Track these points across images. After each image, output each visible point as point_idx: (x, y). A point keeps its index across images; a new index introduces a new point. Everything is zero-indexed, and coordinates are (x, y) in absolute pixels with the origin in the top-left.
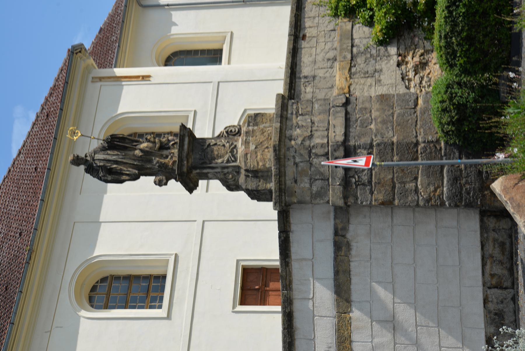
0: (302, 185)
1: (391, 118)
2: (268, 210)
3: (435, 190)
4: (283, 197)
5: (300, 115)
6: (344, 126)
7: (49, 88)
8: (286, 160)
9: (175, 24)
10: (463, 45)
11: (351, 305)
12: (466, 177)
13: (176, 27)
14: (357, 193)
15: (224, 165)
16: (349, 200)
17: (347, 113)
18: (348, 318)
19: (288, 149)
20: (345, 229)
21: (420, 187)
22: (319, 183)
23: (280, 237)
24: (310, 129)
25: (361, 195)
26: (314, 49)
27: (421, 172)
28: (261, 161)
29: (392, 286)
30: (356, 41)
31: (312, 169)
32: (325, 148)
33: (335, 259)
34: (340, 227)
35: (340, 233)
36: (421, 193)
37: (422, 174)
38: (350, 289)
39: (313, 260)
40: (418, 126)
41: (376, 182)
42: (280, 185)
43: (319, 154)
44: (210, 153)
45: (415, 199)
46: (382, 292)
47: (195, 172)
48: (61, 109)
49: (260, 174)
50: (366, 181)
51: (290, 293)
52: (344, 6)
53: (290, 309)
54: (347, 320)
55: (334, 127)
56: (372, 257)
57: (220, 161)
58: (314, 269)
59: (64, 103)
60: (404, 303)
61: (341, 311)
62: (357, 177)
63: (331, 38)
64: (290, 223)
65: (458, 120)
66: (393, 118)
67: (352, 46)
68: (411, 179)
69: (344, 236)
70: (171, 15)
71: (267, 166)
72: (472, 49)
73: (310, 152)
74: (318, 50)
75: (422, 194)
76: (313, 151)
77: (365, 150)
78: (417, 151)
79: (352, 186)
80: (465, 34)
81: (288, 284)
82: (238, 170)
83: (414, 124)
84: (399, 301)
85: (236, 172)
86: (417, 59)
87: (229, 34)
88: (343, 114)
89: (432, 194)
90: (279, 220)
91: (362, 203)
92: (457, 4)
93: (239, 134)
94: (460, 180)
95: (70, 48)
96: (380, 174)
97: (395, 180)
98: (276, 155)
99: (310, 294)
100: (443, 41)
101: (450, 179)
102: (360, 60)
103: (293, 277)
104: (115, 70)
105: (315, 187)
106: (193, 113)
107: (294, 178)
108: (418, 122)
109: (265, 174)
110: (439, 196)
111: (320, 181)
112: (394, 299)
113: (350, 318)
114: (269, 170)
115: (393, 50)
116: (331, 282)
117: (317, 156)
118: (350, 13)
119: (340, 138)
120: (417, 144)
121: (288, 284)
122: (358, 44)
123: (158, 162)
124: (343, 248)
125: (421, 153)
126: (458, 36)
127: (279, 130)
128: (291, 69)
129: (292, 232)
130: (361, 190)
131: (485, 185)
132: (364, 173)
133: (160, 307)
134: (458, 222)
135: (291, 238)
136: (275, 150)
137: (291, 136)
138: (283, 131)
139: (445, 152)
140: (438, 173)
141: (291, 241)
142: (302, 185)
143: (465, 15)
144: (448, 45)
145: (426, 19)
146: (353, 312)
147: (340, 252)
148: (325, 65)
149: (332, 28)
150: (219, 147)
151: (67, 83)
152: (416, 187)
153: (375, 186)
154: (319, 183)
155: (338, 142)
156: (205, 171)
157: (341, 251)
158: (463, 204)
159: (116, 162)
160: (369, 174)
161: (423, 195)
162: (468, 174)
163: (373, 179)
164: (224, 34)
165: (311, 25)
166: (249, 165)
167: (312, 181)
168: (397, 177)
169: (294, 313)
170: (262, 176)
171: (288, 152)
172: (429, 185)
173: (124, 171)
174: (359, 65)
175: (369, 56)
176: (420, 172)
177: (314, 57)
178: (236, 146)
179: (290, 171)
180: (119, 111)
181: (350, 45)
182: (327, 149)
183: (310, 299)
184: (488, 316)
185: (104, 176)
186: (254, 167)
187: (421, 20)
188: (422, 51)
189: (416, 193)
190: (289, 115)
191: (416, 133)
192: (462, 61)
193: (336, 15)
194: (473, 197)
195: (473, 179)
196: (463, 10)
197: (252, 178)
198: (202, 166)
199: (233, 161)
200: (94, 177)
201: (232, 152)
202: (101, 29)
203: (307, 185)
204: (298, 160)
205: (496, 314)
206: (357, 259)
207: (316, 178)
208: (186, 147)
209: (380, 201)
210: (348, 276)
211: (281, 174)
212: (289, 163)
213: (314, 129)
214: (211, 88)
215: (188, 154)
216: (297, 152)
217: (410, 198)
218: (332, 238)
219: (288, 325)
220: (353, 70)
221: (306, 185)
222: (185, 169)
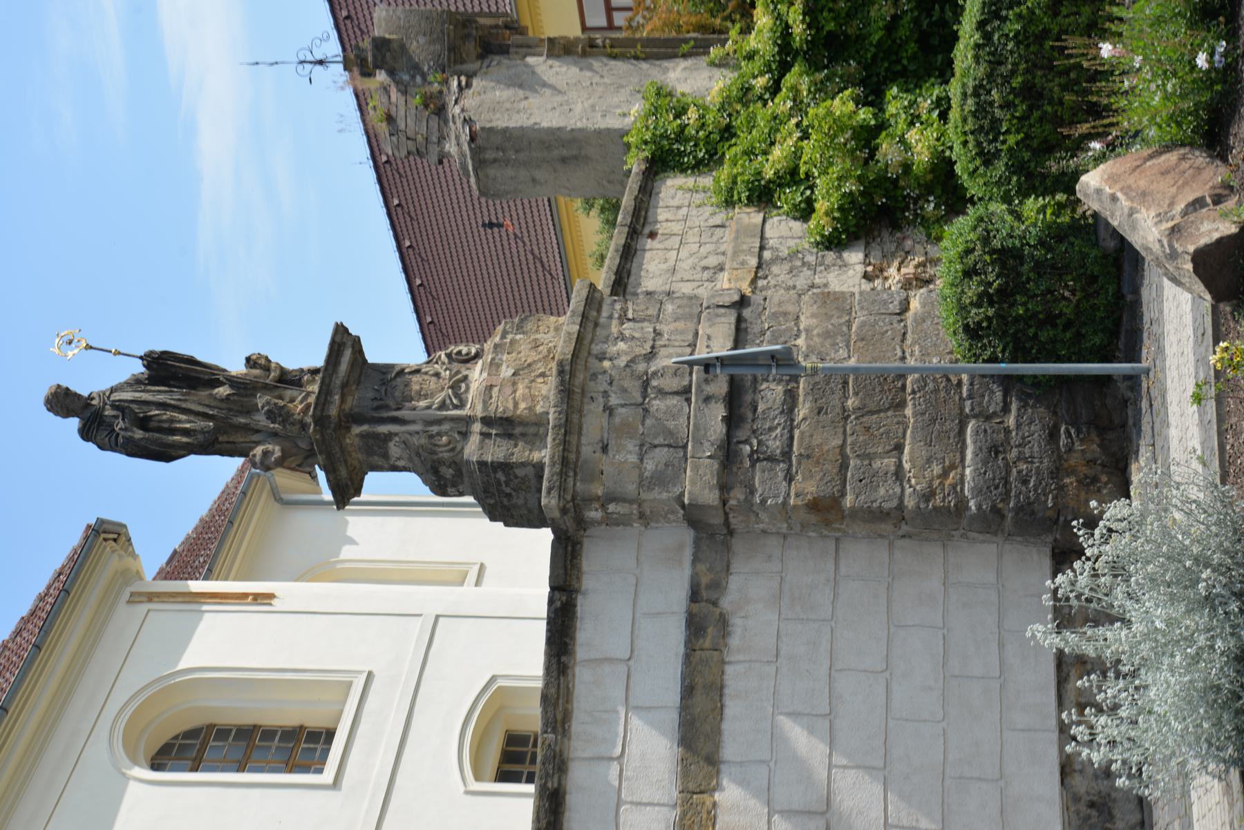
1: (845, 329)
3: (945, 474)
4: (570, 481)
5: (629, 320)
6: (732, 339)
7: (18, 619)
8: (586, 400)
9: (352, 542)
10: (1015, 106)
11: (718, 772)
12: (1020, 445)
13: (353, 547)
14: (753, 478)
16: (732, 494)
17: (739, 319)
18: (709, 804)
19: (594, 376)
20: (718, 586)
21: (907, 466)
22: (662, 454)
23: (551, 602)
24: (650, 343)
25: (763, 482)
26: (675, 252)
27: (912, 432)
28: (524, 399)
29: (828, 724)
30: (771, 242)
31: (648, 422)
32: (682, 376)
33: (688, 658)
34: (704, 580)
35: (704, 594)
36: (909, 480)
37: (913, 438)
38: (719, 732)
39: (631, 663)
40: (909, 341)
41: (801, 455)
42: (564, 450)
43: (667, 389)
44: (402, 387)
45: (895, 493)
46: (799, 737)
47: (357, 430)
48: (37, 647)
49: (518, 430)
50: (778, 451)
51: (562, 742)
52: (748, 182)
53: (559, 784)
54: (704, 811)
55: (709, 338)
56: (782, 653)
57: (423, 404)
58: (631, 684)
59: (47, 633)
60: (858, 767)
61: (691, 786)
62: (755, 442)
63: (715, 238)
64: (579, 570)
65: (1000, 291)
66: (850, 330)
67: (762, 248)
68: (888, 448)
69: (715, 603)
70: (347, 522)
71: (539, 409)
72: (1036, 114)
73: (646, 385)
74: (683, 254)
75: (913, 481)
76: (654, 383)
77: (778, 384)
78: (904, 387)
79: (741, 463)
80: (1020, 79)
81: (559, 717)
82: (464, 429)
83: (899, 338)
84: (845, 762)
85: (459, 433)
86: (909, 270)
87: (477, 568)
88: (733, 319)
89: (936, 483)
90: (551, 622)
91: (764, 501)
92: (1004, 13)
94: (1005, 452)
95: (93, 522)
96: (811, 436)
97: (848, 450)
98: (562, 382)
99: (614, 745)
100: (970, 101)
101: (981, 449)
102: (779, 272)
103: (575, 704)
104: (190, 582)
105: (650, 462)
106: (364, 677)
107: (602, 441)
108: (909, 337)
109: (532, 430)
110: (954, 486)
111: (666, 449)
112: (830, 755)
113: (715, 804)
114: (540, 421)
115: (854, 257)
116: (672, 717)
117: (662, 393)
118: (760, 198)
120: (902, 376)
121: (559, 717)
123: (268, 403)
124: (710, 630)
125: (914, 392)
126: (1003, 85)
128: (616, 274)
129: (584, 594)
130: (764, 471)
131: (1066, 465)
132: (774, 435)
134: (999, 573)
135: (579, 609)
136: (561, 372)
137: (604, 353)
138: (586, 342)
139: (969, 390)
140: (952, 435)
141: (579, 614)
143: (1021, 38)
144: (981, 110)
145: (931, 198)
146: (723, 790)
147: (701, 641)
148: (697, 277)
149: (719, 222)
150: (426, 377)
151: (68, 592)
152: (899, 466)
153: (799, 463)
154: (662, 454)
156: (383, 429)
157: (704, 637)
158: (1011, 505)
159: (163, 406)
160: (786, 436)
161: (915, 484)
162: (1023, 438)
163: (795, 448)
164: (464, 568)
165: (671, 218)
166: (493, 408)
167: (645, 448)
168: (853, 444)
169: (567, 797)
170: (523, 435)
171: (592, 383)
172: (929, 461)
173: (180, 422)
175: (799, 263)
176: (909, 432)
178: (466, 378)
179: (594, 424)
180: (182, 665)
181: (758, 245)
182: (687, 379)
183: (611, 759)
184: (1072, 809)
185: (126, 429)
186: (504, 412)
187: (920, 203)
188: (922, 259)
189: (897, 479)
190: (602, 320)
191: (904, 352)
192: (1012, 140)
193: (729, 203)
194: (1035, 490)
195: (1036, 449)
196: (1018, 27)
197: (498, 439)
199: (456, 407)
200: (101, 448)
201: (455, 387)
202: (175, 552)
203: (633, 458)
204: (614, 400)
205: (1092, 805)
206: (741, 657)
207: (656, 442)
209: (809, 497)
210: (718, 698)
211: (569, 428)
212: (592, 406)
213: (658, 343)
214: (416, 630)
215: (345, 385)
216: (615, 383)
217: (882, 491)
218: (684, 608)
219: (549, 823)
220: (761, 283)
221: (629, 456)
222: (333, 411)
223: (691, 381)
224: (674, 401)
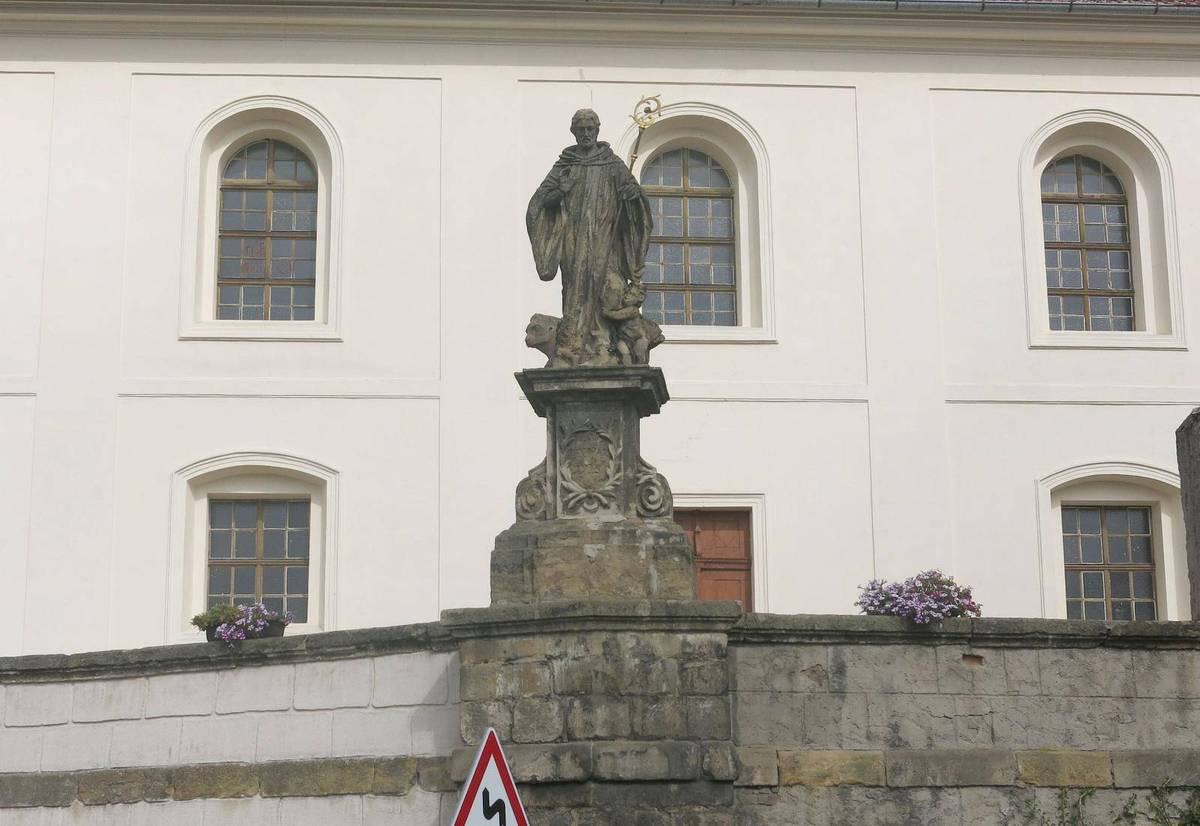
0: (500, 678)
2: (475, 593)
8: (557, 637)
15: (559, 481)
31: (536, 702)
33: (369, 763)
43: (570, 717)
53: (271, 659)
57: (567, 472)
67: (936, 789)
85: (545, 512)
93: (642, 512)
119: (604, 769)
122: (944, 805)
127: (629, 613)
133: (1055, 325)
142: (500, 678)
149: (998, 733)
155: (595, 763)
174: (874, 810)
177: (907, 689)
182: (583, 736)
198: (558, 428)
199: (566, 504)
203: (499, 691)
207: (516, 712)
208: (596, 385)
223: (580, 740)
224: (557, 725)
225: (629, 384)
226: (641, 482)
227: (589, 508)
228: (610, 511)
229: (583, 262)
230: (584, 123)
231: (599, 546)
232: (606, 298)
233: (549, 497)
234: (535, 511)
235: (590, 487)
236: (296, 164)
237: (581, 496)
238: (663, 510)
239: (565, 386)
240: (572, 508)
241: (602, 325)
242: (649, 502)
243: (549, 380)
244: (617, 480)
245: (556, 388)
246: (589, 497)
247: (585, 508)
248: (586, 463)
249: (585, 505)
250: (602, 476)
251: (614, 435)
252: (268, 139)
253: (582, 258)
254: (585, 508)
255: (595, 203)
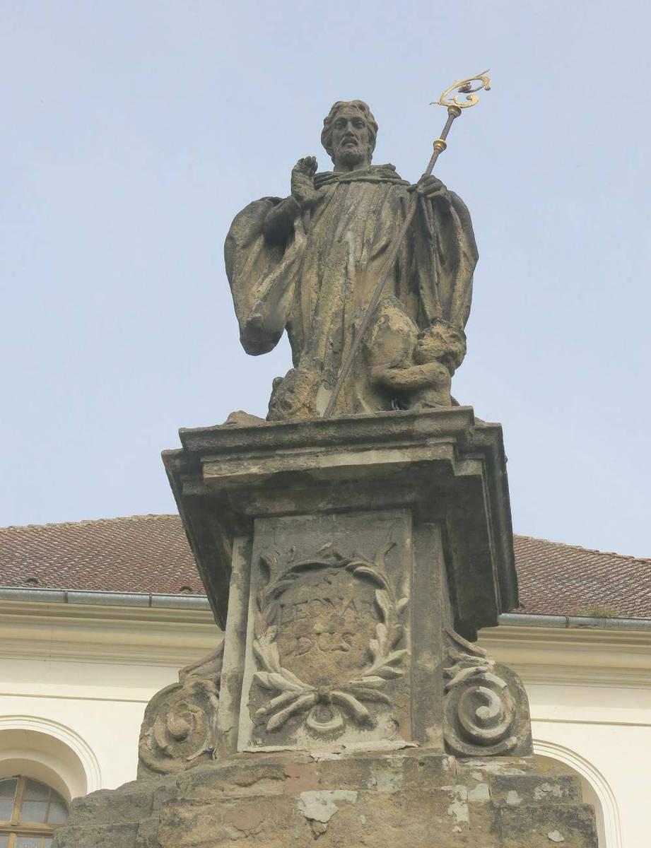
15: (250, 670)
57: (270, 652)
93: (458, 745)
199: (261, 721)
225: (427, 455)
226: (455, 680)
227: (320, 727)
228: (374, 734)
229: (336, 314)
230: (345, 114)
231: (341, 794)
232: (380, 345)
233: (223, 719)
234: (187, 752)
235: (324, 681)
236: (49, 806)
237: (301, 700)
238: (514, 740)
239: (274, 465)
240: (277, 729)
241: (367, 402)
242: (480, 722)
243: (237, 453)
244: (396, 663)
245: (255, 470)
246: (323, 701)
247: (309, 729)
248: (319, 627)
249: (312, 722)
250: (358, 656)
251: (388, 569)
252: (19, 776)
253: (334, 304)
254: (309, 729)
255: (362, 223)
